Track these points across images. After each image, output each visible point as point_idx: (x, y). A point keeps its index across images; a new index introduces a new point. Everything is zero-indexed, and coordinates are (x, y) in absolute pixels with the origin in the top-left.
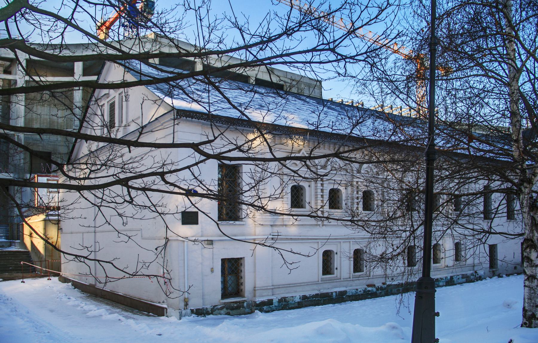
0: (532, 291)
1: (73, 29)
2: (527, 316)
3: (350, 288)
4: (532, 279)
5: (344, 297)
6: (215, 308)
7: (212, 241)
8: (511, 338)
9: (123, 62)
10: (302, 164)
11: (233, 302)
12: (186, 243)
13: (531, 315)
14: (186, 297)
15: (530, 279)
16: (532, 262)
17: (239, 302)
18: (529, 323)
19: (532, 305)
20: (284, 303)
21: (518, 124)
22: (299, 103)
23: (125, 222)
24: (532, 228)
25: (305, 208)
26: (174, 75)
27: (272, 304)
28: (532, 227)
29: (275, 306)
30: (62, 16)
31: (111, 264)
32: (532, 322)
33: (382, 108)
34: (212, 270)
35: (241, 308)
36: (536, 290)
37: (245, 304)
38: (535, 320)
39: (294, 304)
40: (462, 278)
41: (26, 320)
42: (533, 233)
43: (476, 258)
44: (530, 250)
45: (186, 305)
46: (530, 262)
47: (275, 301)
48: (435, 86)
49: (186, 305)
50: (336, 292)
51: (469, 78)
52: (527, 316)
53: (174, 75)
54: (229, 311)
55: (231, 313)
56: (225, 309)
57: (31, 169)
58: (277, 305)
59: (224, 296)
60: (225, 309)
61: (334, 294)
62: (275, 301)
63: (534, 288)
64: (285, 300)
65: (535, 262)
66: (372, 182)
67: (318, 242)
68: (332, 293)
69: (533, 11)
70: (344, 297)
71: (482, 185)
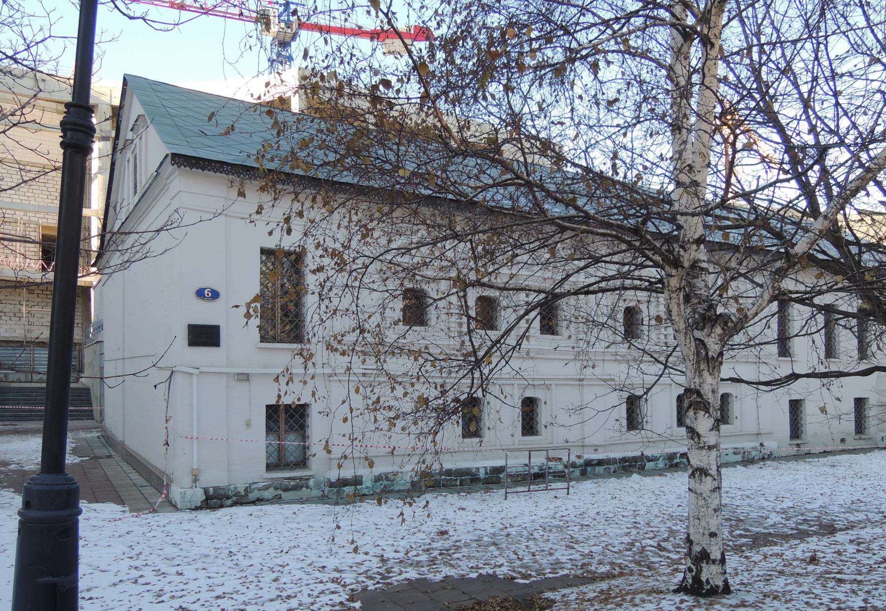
0: (702, 502)
1: (235, 97)
2: (694, 553)
3: (516, 463)
4: (701, 475)
5: (501, 476)
6: (253, 487)
7: (248, 375)
8: (193, 295)
9: (847, 164)
10: (600, 30)
11: (289, 478)
12: (195, 377)
13: (700, 552)
14: (195, 467)
15: (697, 476)
16: (699, 439)
17: (301, 479)
18: (697, 568)
19: (701, 531)
20: (385, 483)
21: (599, 182)
22: (775, 464)
23: (613, 358)
24: (699, 367)
25: (310, 470)
26: (826, 258)
27: (361, 483)
28: (698, 362)
29: (367, 488)
30: (10, 575)
31: (876, 373)
32: (701, 567)
33: (450, 229)
34: (248, 424)
35: (304, 489)
36: (710, 501)
37: (311, 482)
38: (707, 563)
39: (403, 485)
40: (735, 453)
41: (479, 394)
42: (701, 376)
43: (857, 468)
44: (695, 413)
45: (195, 480)
46: (696, 439)
47: (367, 482)
48: (789, 163)
49: (195, 480)
50: (485, 468)
51: (700, 231)
52: (694, 553)
53: (826, 258)
54: (279, 492)
55: (283, 496)
56: (271, 490)
57: (315, 182)
58: (370, 485)
59: (269, 467)
60: (271, 490)
61: (482, 472)
62: (367, 482)
63: (704, 495)
64: (387, 478)
65: (706, 439)
66: (860, 582)
67: (513, 385)
68: (478, 469)
69: (617, 43)
70: (501, 476)
71: (810, 554)
